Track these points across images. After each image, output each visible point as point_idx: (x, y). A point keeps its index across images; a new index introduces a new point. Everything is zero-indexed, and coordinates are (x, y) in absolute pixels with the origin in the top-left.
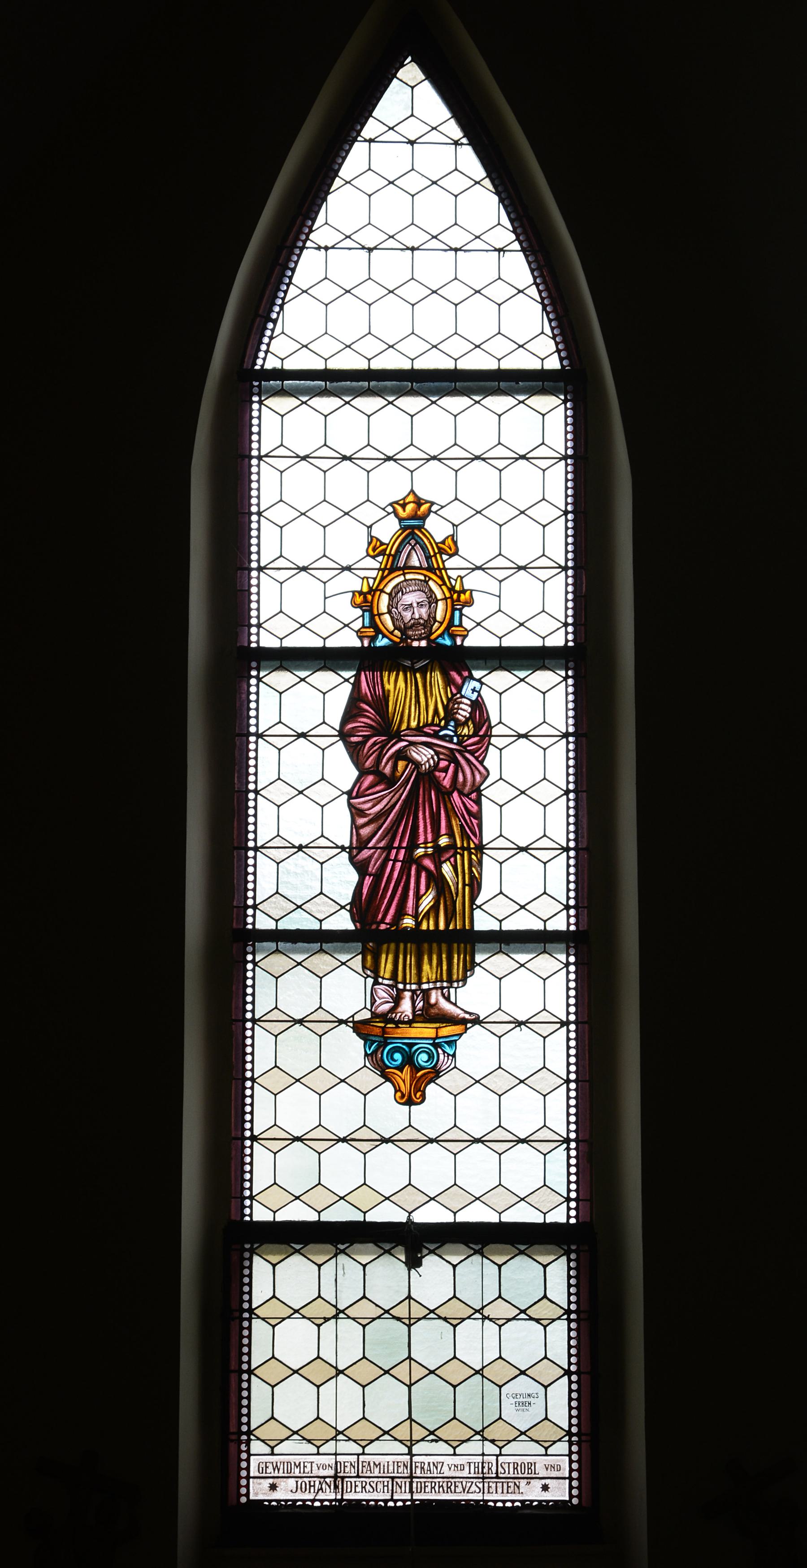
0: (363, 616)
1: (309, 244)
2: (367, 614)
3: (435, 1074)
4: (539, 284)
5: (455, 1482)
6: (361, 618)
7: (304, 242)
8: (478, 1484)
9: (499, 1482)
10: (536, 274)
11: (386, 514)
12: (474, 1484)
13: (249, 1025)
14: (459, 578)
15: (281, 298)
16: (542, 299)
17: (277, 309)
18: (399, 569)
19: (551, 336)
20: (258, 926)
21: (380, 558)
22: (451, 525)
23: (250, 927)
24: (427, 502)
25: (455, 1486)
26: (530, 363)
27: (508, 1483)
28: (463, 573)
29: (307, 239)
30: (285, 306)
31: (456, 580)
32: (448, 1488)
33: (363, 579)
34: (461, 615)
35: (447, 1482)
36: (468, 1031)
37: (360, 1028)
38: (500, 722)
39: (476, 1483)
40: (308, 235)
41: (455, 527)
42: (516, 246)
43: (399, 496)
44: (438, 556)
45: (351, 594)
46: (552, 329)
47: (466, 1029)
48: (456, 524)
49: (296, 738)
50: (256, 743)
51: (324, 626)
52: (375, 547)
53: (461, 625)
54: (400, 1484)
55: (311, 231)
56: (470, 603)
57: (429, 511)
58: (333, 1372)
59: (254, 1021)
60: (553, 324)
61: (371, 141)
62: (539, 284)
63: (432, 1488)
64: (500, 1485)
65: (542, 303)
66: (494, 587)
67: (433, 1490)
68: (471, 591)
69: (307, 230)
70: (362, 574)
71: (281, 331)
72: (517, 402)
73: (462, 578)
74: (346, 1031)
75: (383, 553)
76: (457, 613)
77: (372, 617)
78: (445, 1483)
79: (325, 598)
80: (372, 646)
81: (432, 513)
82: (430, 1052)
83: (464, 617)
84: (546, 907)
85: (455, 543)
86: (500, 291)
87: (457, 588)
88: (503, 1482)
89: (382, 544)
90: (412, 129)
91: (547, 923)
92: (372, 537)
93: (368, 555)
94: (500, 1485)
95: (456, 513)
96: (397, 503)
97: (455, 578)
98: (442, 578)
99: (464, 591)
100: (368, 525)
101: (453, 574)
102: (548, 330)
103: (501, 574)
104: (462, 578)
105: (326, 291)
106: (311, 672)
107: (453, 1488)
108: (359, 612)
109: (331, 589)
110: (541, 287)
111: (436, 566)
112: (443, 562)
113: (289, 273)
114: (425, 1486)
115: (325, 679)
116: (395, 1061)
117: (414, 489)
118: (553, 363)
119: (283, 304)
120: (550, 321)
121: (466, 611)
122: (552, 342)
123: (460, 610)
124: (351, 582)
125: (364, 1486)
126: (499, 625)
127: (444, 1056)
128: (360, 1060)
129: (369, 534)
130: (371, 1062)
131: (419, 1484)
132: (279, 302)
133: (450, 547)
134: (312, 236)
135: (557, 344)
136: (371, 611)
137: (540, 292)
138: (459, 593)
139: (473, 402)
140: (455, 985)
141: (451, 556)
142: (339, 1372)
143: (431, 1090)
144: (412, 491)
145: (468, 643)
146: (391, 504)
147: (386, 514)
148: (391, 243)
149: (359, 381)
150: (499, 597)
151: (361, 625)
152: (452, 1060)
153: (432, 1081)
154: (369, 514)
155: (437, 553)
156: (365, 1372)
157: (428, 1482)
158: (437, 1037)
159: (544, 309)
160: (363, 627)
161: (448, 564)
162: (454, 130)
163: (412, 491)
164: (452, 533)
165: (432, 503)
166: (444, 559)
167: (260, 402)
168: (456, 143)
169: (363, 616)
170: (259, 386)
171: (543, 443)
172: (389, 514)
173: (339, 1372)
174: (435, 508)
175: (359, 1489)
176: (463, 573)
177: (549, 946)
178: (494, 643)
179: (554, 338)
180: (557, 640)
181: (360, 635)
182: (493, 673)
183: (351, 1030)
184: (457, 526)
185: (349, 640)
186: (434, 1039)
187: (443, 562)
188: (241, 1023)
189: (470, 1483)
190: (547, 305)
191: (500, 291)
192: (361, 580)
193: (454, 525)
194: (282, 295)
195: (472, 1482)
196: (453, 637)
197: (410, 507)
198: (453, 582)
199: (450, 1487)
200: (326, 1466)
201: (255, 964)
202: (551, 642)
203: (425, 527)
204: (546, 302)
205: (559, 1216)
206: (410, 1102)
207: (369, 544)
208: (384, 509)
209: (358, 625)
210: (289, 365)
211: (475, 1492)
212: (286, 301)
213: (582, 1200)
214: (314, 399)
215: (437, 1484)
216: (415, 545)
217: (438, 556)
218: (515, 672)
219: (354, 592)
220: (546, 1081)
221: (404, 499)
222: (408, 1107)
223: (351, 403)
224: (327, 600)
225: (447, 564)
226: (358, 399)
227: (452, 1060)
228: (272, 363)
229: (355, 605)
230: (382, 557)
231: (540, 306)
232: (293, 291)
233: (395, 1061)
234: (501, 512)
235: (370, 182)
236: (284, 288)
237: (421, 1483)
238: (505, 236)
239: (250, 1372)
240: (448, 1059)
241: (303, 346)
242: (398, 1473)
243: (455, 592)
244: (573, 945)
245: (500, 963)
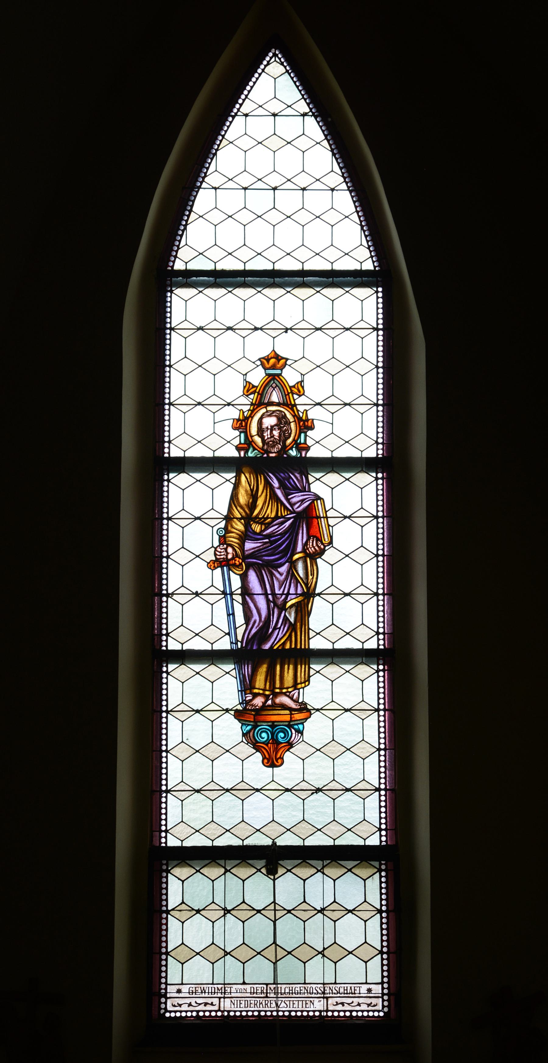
0: (240, 436)
1: (204, 185)
2: (242, 435)
3: (290, 745)
4: (359, 212)
5: (270, 1001)
6: (239, 437)
7: (201, 183)
8: (286, 1002)
9: (300, 1001)
10: (356, 204)
11: (256, 366)
12: (283, 1002)
13: (164, 715)
14: (305, 412)
15: (185, 220)
16: (361, 221)
17: (182, 228)
18: (264, 404)
19: (367, 247)
20: (170, 648)
21: (252, 396)
22: (300, 374)
23: (164, 648)
24: (283, 358)
25: (271, 1003)
26: (351, 265)
27: (306, 1001)
28: (307, 407)
29: (203, 181)
30: (188, 227)
31: (303, 413)
32: (265, 1004)
33: (240, 411)
34: (306, 436)
35: (265, 1001)
36: (312, 716)
37: (238, 715)
38: (332, 508)
39: (284, 1001)
40: (204, 178)
41: (302, 376)
42: (344, 186)
43: (264, 354)
44: (290, 395)
45: (232, 420)
46: (368, 241)
47: (311, 714)
48: (304, 374)
49: (194, 520)
50: (378, 400)
51: (214, 442)
52: (249, 389)
53: (305, 443)
54: (233, 1002)
55: (206, 176)
56: (312, 428)
57: (285, 364)
58: (222, 953)
59: (167, 712)
60: (368, 238)
61: (246, 115)
62: (359, 212)
63: (255, 1004)
64: (300, 1003)
65: (361, 225)
66: (328, 417)
67: (256, 1005)
68: (313, 420)
69: (203, 175)
70: (240, 407)
71: (185, 244)
72: (345, 292)
73: (307, 411)
74: (229, 718)
75: (254, 393)
76: (303, 435)
77: (246, 437)
78: (264, 1001)
79: (215, 423)
80: (247, 456)
81: (287, 366)
82: (279, 730)
83: (307, 437)
84: (363, 633)
85: (303, 387)
86: (332, 217)
87: (304, 418)
88: (302, 1001)
89: (253, 386)
90: (275, 107)
91: (364, 644)
92: (246, 382)
93: (244, 394)
94: (300, 1003)
95: (303, 366)
96: (263, 358)
97: (302, 411)
98: (293, 411)
99: (307, 420)
100: (244, 374)
101: (301, 408)
102: (365, 243)
103: (333, 409)
104: (307, 411)
105: (216, 217)
106: (208, 474)
107: (269, 1004)
108: (237, 433)
109: (218, 417)
110: (360, 214)
111: (289, 403)
112: (294, 400)
113: (191, 203)
114: (250, 1003)
115: (213, 479)
116: (263, 738)
117: (275, 349)
118: (369, 266)
119: (186, 224)
120: (366, 236)
121: (309, 433)
122: (368, 250)
123: (305, 433)
124: (234, 413)
125: (256, 1003)
126: (332, 442)
127: (296, 735)
128: (239, 737)
129: (245, 380)
130: (247, 739)
131: (246, 1002)
132: (184, 223)
133: (299, 389)
134: (206, 179)
135: (371, 252)
136: (246, 433)
137: (359, 217)
138: (304, 421)
139: (316, 292)
140: (299, 686)
141: (300, 396)
142: (226, 953)
143: (288, 756)
144: (274, 350)
145: (310, 454)
146: (260, 359)
147: (256, 366)
148: (260, 185)
149: (237, 278)
150: (332, 424)
151: (238, 443)
152: (301, 737)
153: (288, 750)
154: (244, 366)
155: (290, 393)
156: (244, 953)
157: (243, 1000)
158: (291, 721)
159: (362, 228)
160: (240, 443)
161: (297, 402)
162: (303, 107)
163: (274, 350)
164: (300, 380)
165: (287, 359)
166: (295, 398)
167: (171, 292)
168: (304, 115)
169: (240, 436)
170: (171, 280)
171: (274, 338)
172: (258, 366)
173: (226, 953)
174: (289, 362)
175: (242, 1005)
176: (307, 407)
177: (335, 660)
178: (328, 454)
179: (369, 248)
180: (371, 453)
181: (238, 448)
182: (328, 475)
183: (233, 717)
184: (304, 375)
185: (230, 452)
186: (289, 722)
187: (294, 400)
188: (159, 713)
189: (281, 1001)
190: (364, 226)
191: (332, 217)
192: (239, 411)
193: (302, 374)
194: (186, 218)
195: (282, 1001)
196: (299, 449)
197: (272, 361)
198: (301, 415)
199: (267, 1004)
200: (242, 990)
201: (168, 673)
202: (367, 454)
203: (283, 375)
204: (363, 224)
205: (374, 841)
206: (273, 765)
207: (244, 387)
208: (254, 363)
209: (236, 442)
210: (191, 266)
211: (284, 1007)
212: (188, 223)
213: (389, 830)
214: (206, 290)
215: (258, 1002)
216: (275, 387)
217: (290, 395)
218: (342, 474)
219: (234, 419)
220: (364, 750)
221: (268, 356)
222: (272, 769)
223: (232, 292)
224: (215, 424)
225: (297, 402)
226: (237, 289)
227: (301, 737)
228: (179, 265)
229: (235, 428)
230: (253, 395)
231: (359, 227)
232: (193, 216)
233: (263, 738)
234: (333, 367)
235: (245, 143)
236: (187, 213)
237: (248, 1001)
238: (336, 179)
239: (167, 953)
240: (298, 736)
241: (229, 217)
242: (240, 1007)
243: (302, 420)
244: (381, 658)
245: (332, 670)
